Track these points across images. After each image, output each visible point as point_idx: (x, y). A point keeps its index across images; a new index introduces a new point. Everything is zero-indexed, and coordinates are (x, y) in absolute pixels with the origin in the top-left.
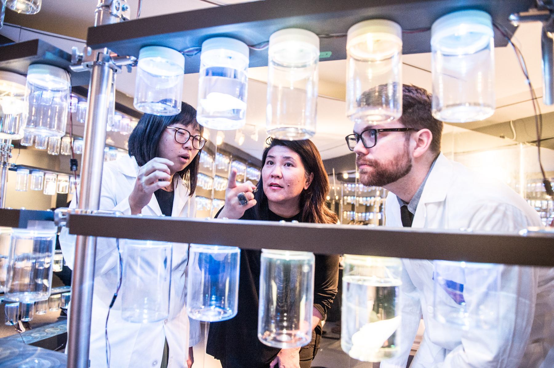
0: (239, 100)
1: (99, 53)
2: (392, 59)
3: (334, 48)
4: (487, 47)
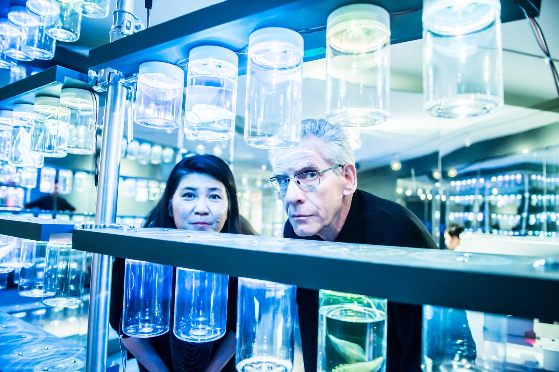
0: (230, 112)
1: (110, 73)
2: (375, 53)
3: (315, 42)
4: (492, 24)
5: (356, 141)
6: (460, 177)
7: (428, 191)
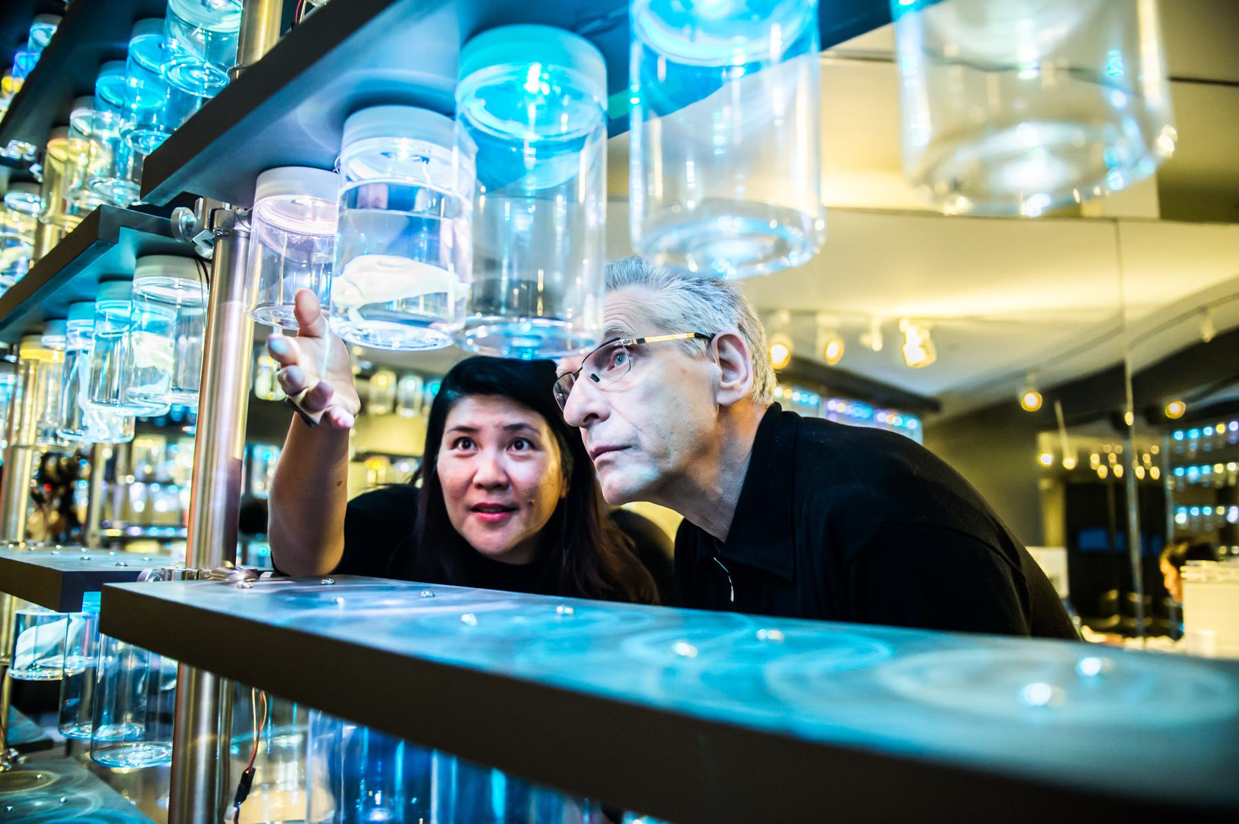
1: (213, 211)
5: (923, 346)
6: (1191, 420)
7: (1113, 459)
